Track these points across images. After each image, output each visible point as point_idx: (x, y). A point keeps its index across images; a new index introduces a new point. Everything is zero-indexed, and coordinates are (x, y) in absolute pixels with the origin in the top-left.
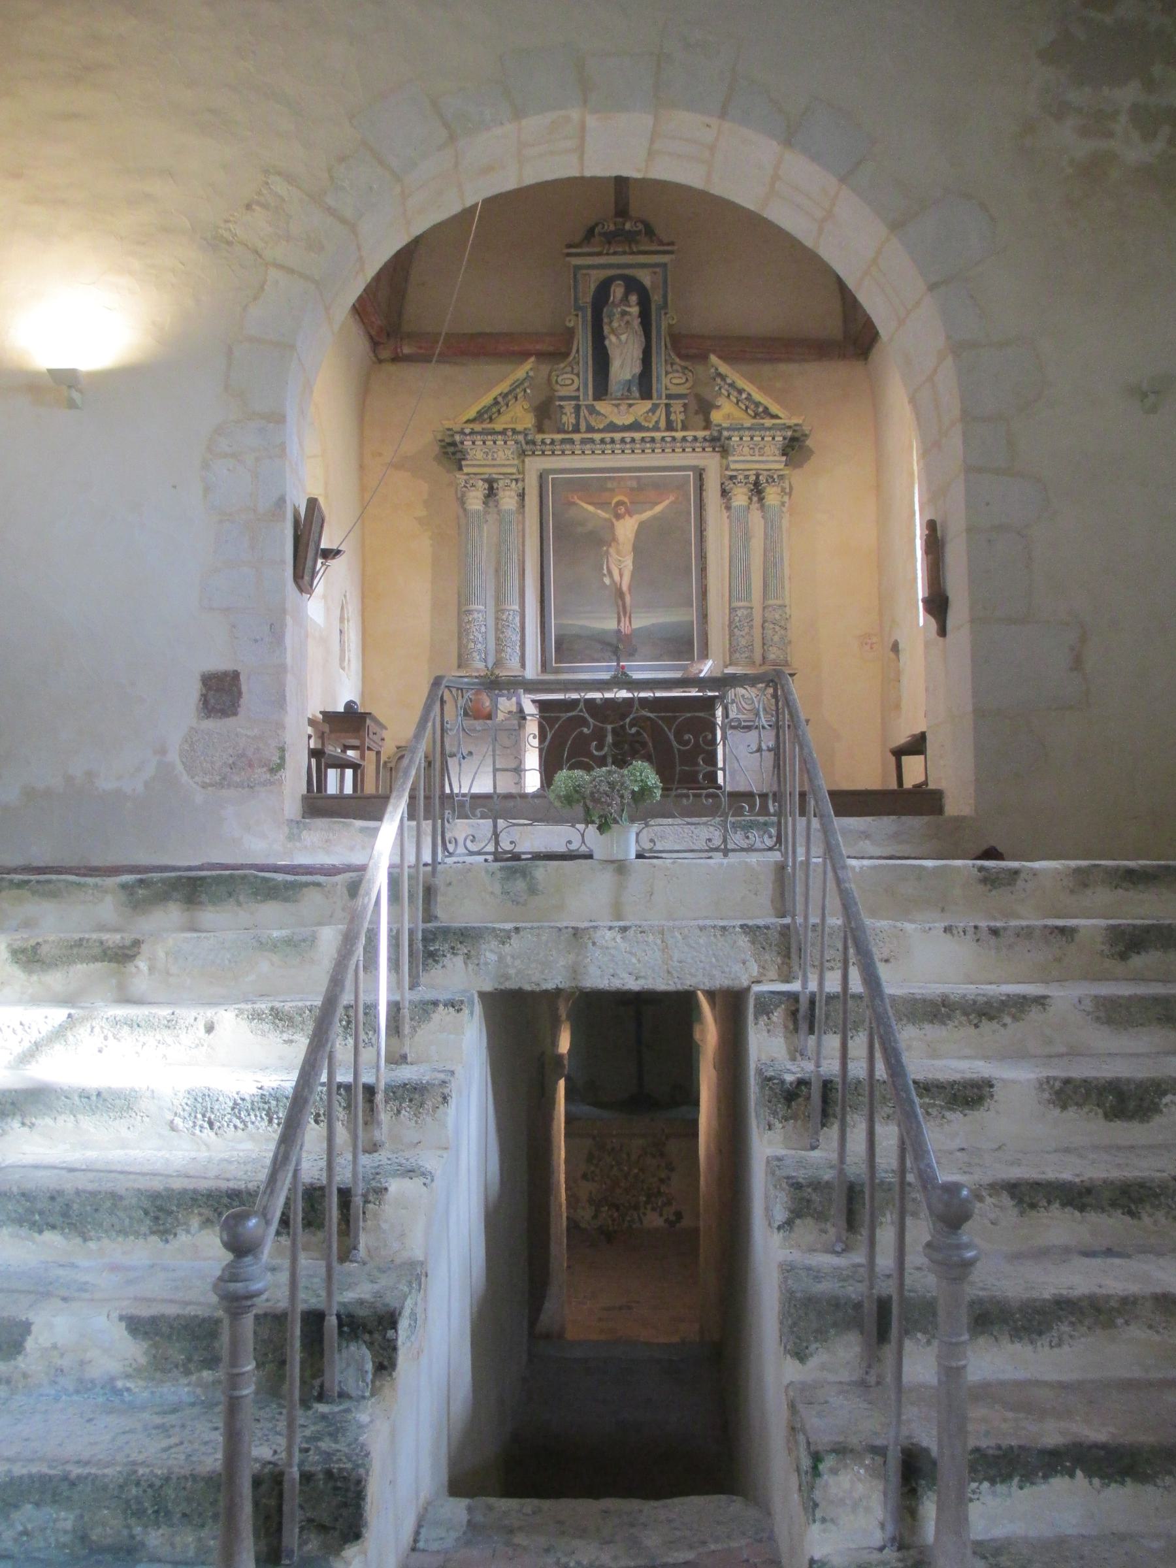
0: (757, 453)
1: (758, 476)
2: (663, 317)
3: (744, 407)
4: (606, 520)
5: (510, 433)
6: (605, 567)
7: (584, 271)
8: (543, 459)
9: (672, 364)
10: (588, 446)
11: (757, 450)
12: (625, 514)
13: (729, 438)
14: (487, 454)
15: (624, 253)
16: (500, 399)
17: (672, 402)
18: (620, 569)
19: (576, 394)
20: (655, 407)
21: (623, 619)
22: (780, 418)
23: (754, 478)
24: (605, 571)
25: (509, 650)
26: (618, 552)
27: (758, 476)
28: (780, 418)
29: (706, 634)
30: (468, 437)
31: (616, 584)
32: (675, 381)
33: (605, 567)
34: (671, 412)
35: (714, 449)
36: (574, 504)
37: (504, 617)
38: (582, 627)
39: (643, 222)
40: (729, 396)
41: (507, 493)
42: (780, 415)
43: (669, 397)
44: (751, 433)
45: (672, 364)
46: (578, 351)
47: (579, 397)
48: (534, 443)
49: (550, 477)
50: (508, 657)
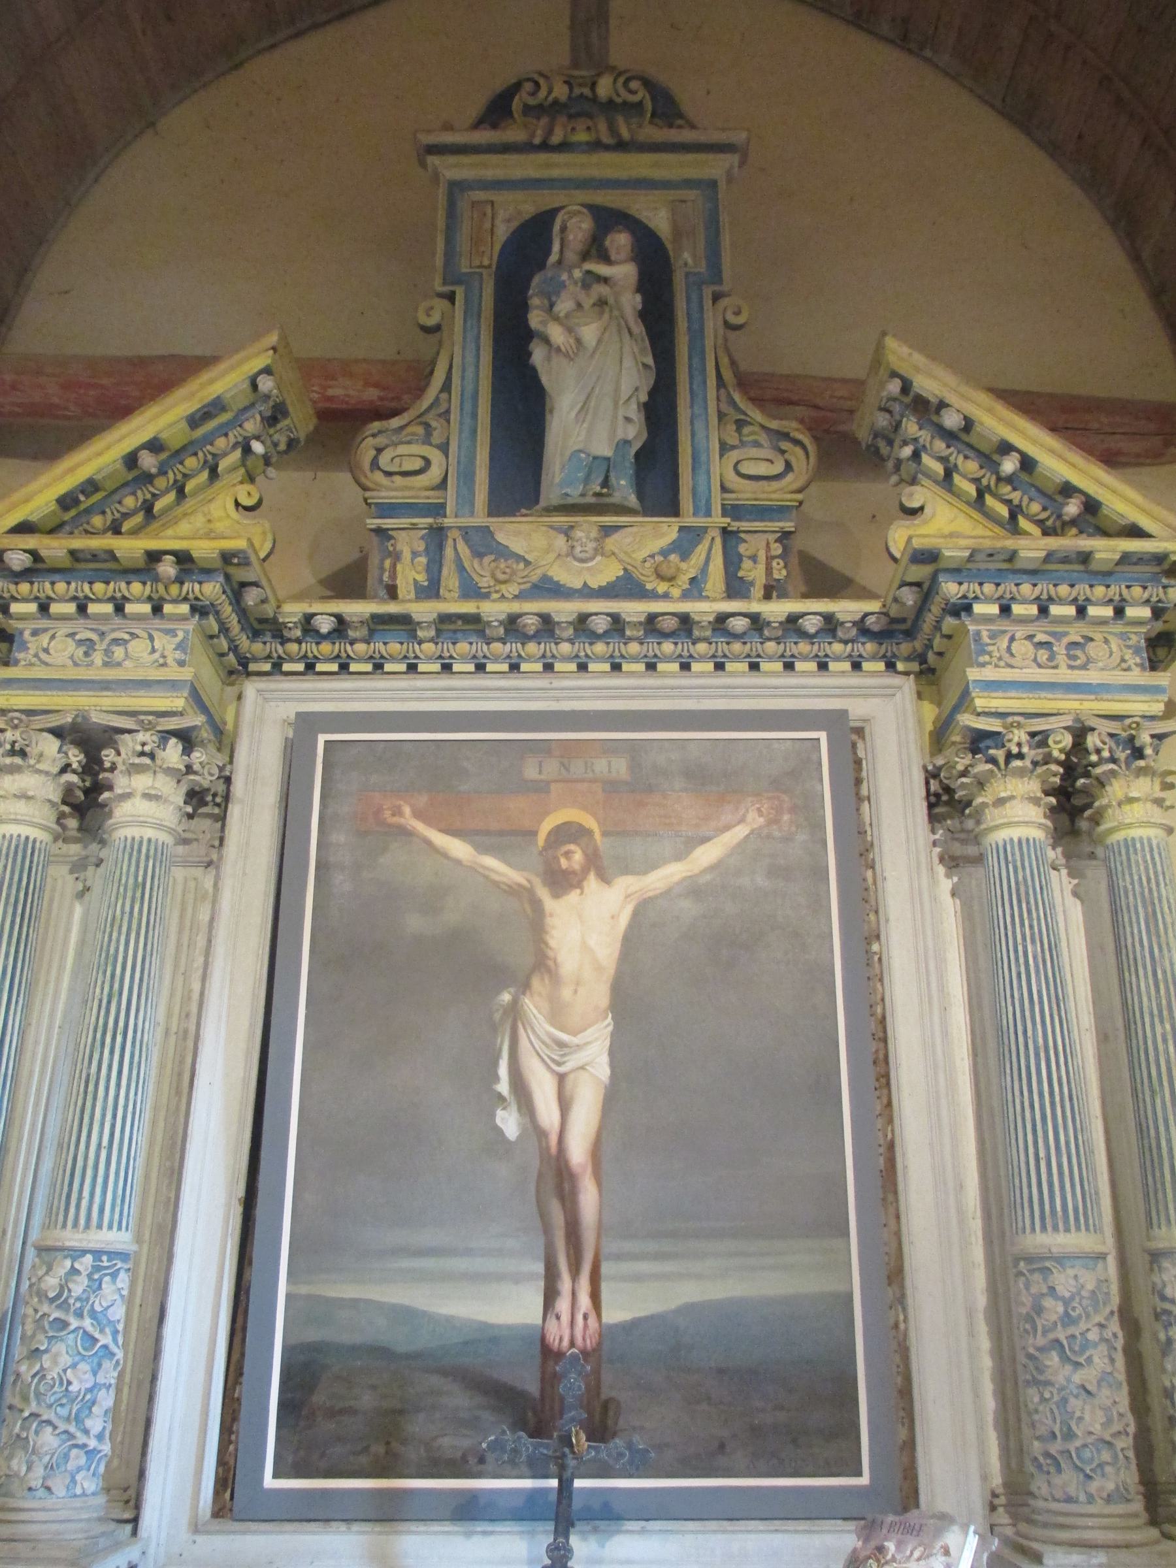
0: (1061, 659)
1: (1080, 733)
2: (707, 303)
3: (1004, 511)
4: (514, 891)
5: (167, 568)
6: (503, 1070)
7: (479, 195)
8: (309, 684)
9: (740, 424)
10: (463, 647)
11: (1060, 649)
12: (585, 871)
13: (962, 608)
14: (89, 645)
15: (597, 146)
16: (148, 461)
17: (745, 525)
18: (561, 1079)
19: (434, 498)
20: (689, 539)
21: (565, 1284)
22: (1148, 536)
23: (1068, 740)
24: (503, 1087)
25: (48, 1440)
26: (556, 1015)
27: (1080, 733)
28: (1148, 536)
29: (904, 1352)
30: (24, 587)
31: (541, 1134)
32: (749, 468)
33: (503, 1070)
34: (740, 558)
35: (891, 666)
36: (406, 833)
37: (51, 1283)
38: (405, 1315)
39: (647, 83)
40: (948, 474)
41: (142, 782)
42: (1145, 523)
43: (733, 511)
44: (1044, 588)
45: (740, 424)
46: (447, 387)
47: (443, 506)
48: (278, 631)
49: (322, 739)
50: (36, 1477)
